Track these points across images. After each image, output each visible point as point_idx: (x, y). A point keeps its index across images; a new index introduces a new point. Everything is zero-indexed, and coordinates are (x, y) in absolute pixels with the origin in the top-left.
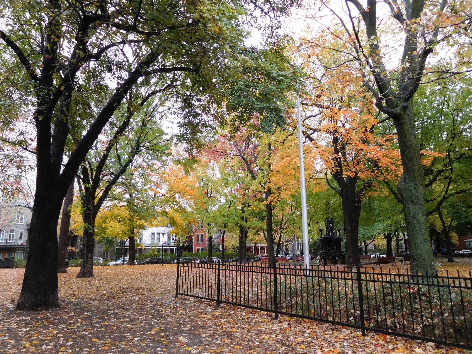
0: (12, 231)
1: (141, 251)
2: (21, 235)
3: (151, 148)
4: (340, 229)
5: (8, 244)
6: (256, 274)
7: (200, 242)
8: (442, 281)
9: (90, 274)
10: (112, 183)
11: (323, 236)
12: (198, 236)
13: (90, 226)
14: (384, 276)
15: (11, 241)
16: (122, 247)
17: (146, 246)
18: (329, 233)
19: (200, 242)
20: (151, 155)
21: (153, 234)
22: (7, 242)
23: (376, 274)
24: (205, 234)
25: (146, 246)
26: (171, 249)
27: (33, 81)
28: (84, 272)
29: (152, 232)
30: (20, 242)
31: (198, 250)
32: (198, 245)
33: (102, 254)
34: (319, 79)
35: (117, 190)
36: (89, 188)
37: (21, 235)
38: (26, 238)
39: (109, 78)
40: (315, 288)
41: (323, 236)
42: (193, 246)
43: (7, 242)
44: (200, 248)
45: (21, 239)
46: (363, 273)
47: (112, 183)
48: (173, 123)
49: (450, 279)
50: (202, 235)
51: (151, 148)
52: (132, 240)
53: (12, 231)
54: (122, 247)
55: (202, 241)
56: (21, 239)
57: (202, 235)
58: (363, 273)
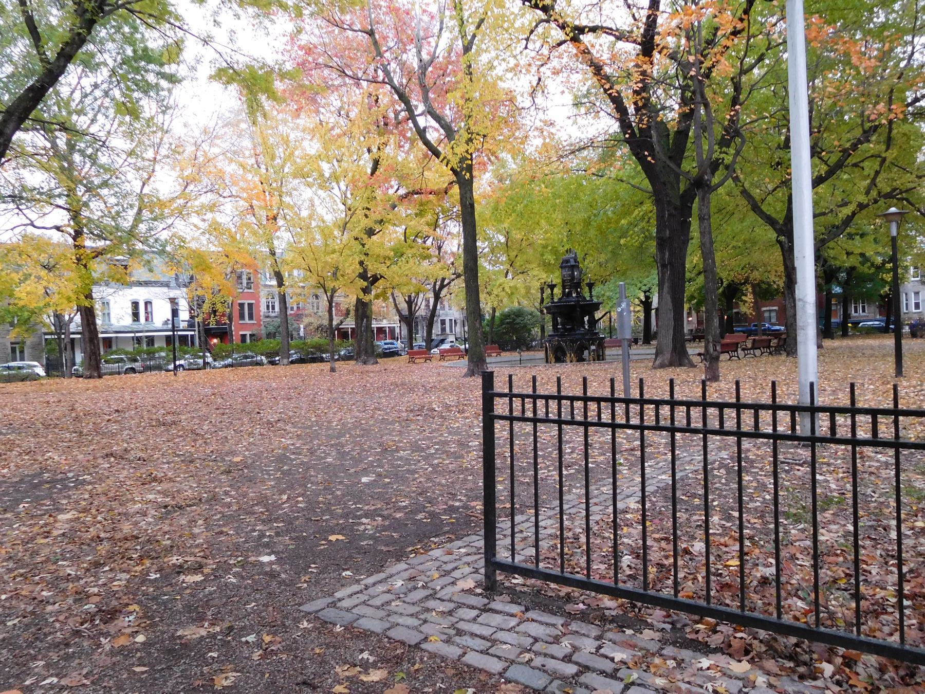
1: (108, 342)
4: (555, 286)
6: (529, 427)
7: (247, 320)
8: (506, 434)
11: (556, 300)
12: (242, 305)
14: (697, 424)
16: (59, 334)
18: (570, 294)
19: (247, 320)
21: (135, 305)
23: (517, 396)
24: (258, 302)
31: (244, 336)
32: (244, 327)
33: (10, 350)
40: (654, 556)
41: (556, 300)
44: (248, 333)
46: (501, 395)
49: (646, 432)
50: (250, 305)
54: (59, 334)
55: (251, 318)
57: (250, 305)
58: (501, 395)
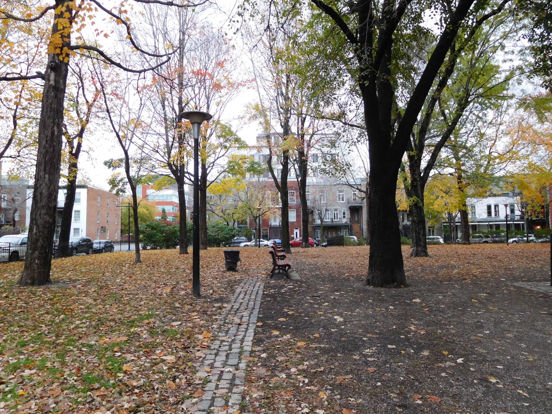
0: (336, 210)
1: (474, 227)
2: (344, 213)
3: (486, 94)
5: (334, 223)
9: (424, 254)
10: (438, 147)
13: (419, 200)
15: (336, 220)
16: (450, 223)
17: (479, 222)
20: (480, 104)
21: (489, 207)
22: (332, 221)
25: (479, 222)
26: (515, 224)
27: (354, 44)
28: (417, 251)
29: (488, 203)
30: (344, 221)
34: (132, 130)
35: (444, 153)
36: (413, 156)
37: (344, 213)
38: (349, 216)
39: (430, 16)
42: (550, 220)
43: (332, 221)
45: (344, 217)
47: (438, 147)
48: (513, 52)
51: (486, 94)
52: (464, 214)
53: (336, 210)
56: (344, 217)
